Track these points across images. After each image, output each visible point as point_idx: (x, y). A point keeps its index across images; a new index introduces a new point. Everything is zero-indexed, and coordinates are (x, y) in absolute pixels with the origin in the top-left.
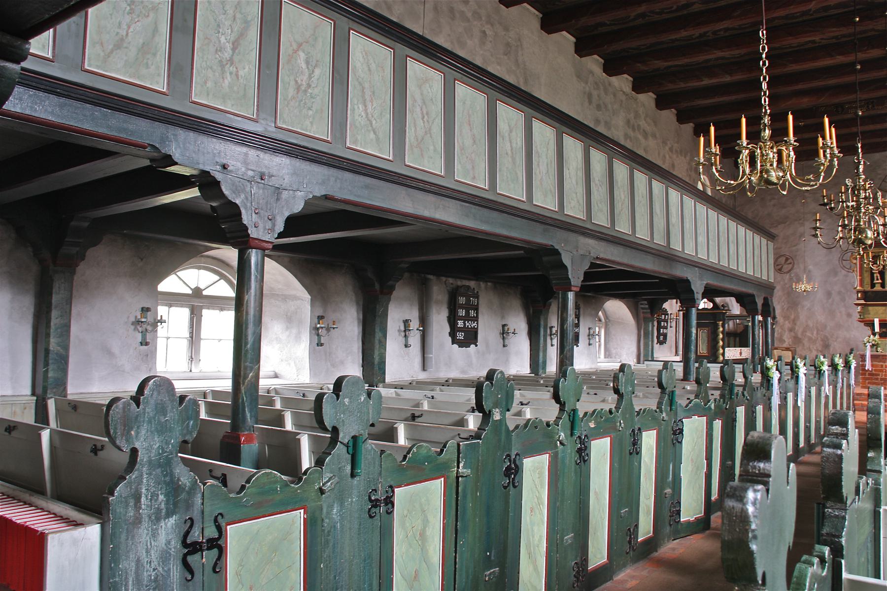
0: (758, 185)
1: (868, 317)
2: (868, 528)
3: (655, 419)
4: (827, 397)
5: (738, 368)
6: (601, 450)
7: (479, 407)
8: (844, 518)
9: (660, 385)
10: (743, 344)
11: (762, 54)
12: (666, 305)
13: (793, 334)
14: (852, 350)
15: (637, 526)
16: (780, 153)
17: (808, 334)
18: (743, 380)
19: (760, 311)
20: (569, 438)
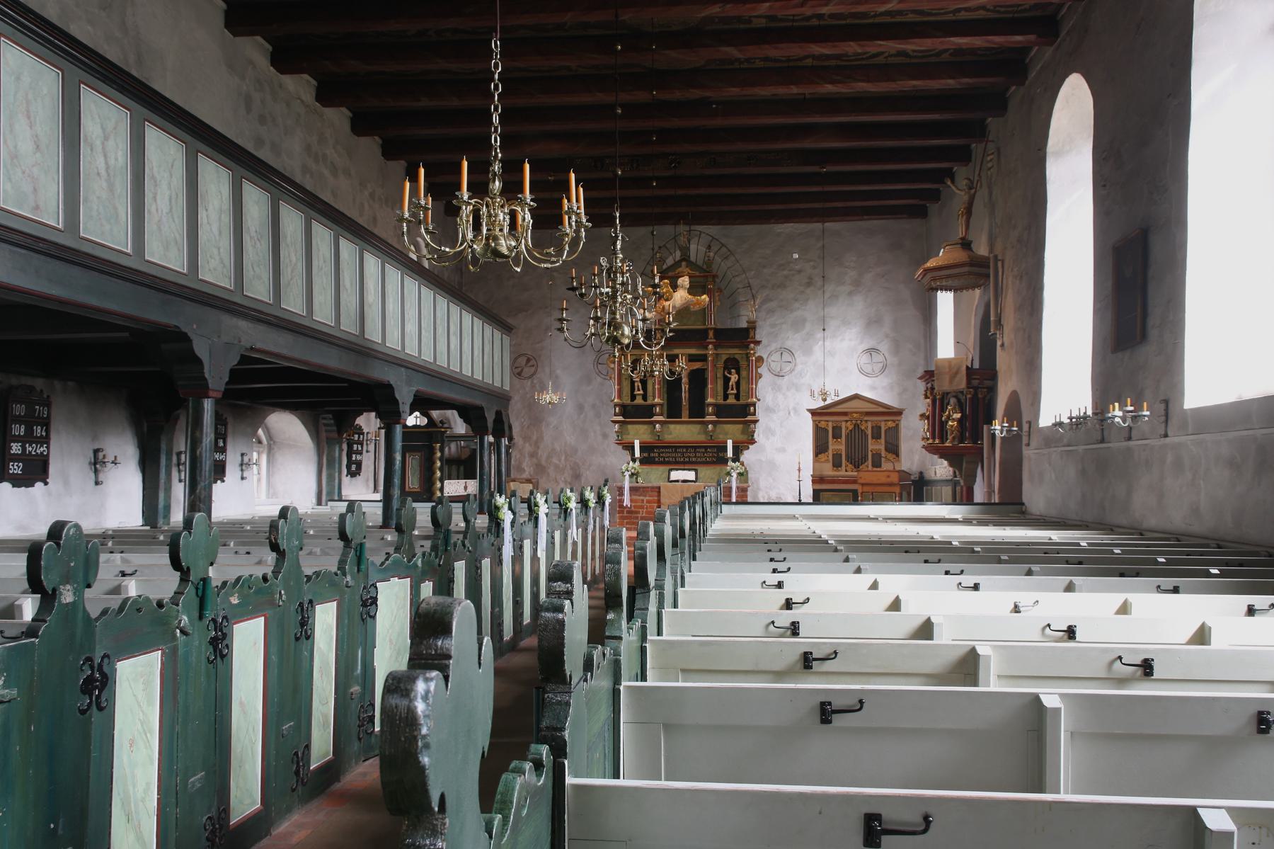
0: (484, 255)
1: (627, 439)
2: (605, 712)
3: (333, 584)
4: (575, 543)
5: (457, 508)
6: (249, 640)
7: (35, 583)
8: (568, 704)
9: (343, 536)
10: (469, 475)
11: (493, 74)
12: (361, 421)
13: (535, 460)
14: (606, 481)
15: (308, 747)
16: (513, 215)
17: (555, 460)
18: (463, 525)
19: (490, 430)
20: (197, 622)
